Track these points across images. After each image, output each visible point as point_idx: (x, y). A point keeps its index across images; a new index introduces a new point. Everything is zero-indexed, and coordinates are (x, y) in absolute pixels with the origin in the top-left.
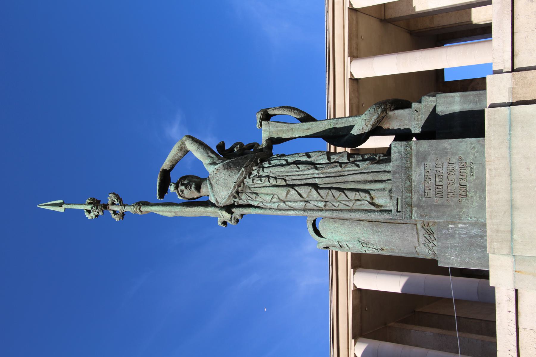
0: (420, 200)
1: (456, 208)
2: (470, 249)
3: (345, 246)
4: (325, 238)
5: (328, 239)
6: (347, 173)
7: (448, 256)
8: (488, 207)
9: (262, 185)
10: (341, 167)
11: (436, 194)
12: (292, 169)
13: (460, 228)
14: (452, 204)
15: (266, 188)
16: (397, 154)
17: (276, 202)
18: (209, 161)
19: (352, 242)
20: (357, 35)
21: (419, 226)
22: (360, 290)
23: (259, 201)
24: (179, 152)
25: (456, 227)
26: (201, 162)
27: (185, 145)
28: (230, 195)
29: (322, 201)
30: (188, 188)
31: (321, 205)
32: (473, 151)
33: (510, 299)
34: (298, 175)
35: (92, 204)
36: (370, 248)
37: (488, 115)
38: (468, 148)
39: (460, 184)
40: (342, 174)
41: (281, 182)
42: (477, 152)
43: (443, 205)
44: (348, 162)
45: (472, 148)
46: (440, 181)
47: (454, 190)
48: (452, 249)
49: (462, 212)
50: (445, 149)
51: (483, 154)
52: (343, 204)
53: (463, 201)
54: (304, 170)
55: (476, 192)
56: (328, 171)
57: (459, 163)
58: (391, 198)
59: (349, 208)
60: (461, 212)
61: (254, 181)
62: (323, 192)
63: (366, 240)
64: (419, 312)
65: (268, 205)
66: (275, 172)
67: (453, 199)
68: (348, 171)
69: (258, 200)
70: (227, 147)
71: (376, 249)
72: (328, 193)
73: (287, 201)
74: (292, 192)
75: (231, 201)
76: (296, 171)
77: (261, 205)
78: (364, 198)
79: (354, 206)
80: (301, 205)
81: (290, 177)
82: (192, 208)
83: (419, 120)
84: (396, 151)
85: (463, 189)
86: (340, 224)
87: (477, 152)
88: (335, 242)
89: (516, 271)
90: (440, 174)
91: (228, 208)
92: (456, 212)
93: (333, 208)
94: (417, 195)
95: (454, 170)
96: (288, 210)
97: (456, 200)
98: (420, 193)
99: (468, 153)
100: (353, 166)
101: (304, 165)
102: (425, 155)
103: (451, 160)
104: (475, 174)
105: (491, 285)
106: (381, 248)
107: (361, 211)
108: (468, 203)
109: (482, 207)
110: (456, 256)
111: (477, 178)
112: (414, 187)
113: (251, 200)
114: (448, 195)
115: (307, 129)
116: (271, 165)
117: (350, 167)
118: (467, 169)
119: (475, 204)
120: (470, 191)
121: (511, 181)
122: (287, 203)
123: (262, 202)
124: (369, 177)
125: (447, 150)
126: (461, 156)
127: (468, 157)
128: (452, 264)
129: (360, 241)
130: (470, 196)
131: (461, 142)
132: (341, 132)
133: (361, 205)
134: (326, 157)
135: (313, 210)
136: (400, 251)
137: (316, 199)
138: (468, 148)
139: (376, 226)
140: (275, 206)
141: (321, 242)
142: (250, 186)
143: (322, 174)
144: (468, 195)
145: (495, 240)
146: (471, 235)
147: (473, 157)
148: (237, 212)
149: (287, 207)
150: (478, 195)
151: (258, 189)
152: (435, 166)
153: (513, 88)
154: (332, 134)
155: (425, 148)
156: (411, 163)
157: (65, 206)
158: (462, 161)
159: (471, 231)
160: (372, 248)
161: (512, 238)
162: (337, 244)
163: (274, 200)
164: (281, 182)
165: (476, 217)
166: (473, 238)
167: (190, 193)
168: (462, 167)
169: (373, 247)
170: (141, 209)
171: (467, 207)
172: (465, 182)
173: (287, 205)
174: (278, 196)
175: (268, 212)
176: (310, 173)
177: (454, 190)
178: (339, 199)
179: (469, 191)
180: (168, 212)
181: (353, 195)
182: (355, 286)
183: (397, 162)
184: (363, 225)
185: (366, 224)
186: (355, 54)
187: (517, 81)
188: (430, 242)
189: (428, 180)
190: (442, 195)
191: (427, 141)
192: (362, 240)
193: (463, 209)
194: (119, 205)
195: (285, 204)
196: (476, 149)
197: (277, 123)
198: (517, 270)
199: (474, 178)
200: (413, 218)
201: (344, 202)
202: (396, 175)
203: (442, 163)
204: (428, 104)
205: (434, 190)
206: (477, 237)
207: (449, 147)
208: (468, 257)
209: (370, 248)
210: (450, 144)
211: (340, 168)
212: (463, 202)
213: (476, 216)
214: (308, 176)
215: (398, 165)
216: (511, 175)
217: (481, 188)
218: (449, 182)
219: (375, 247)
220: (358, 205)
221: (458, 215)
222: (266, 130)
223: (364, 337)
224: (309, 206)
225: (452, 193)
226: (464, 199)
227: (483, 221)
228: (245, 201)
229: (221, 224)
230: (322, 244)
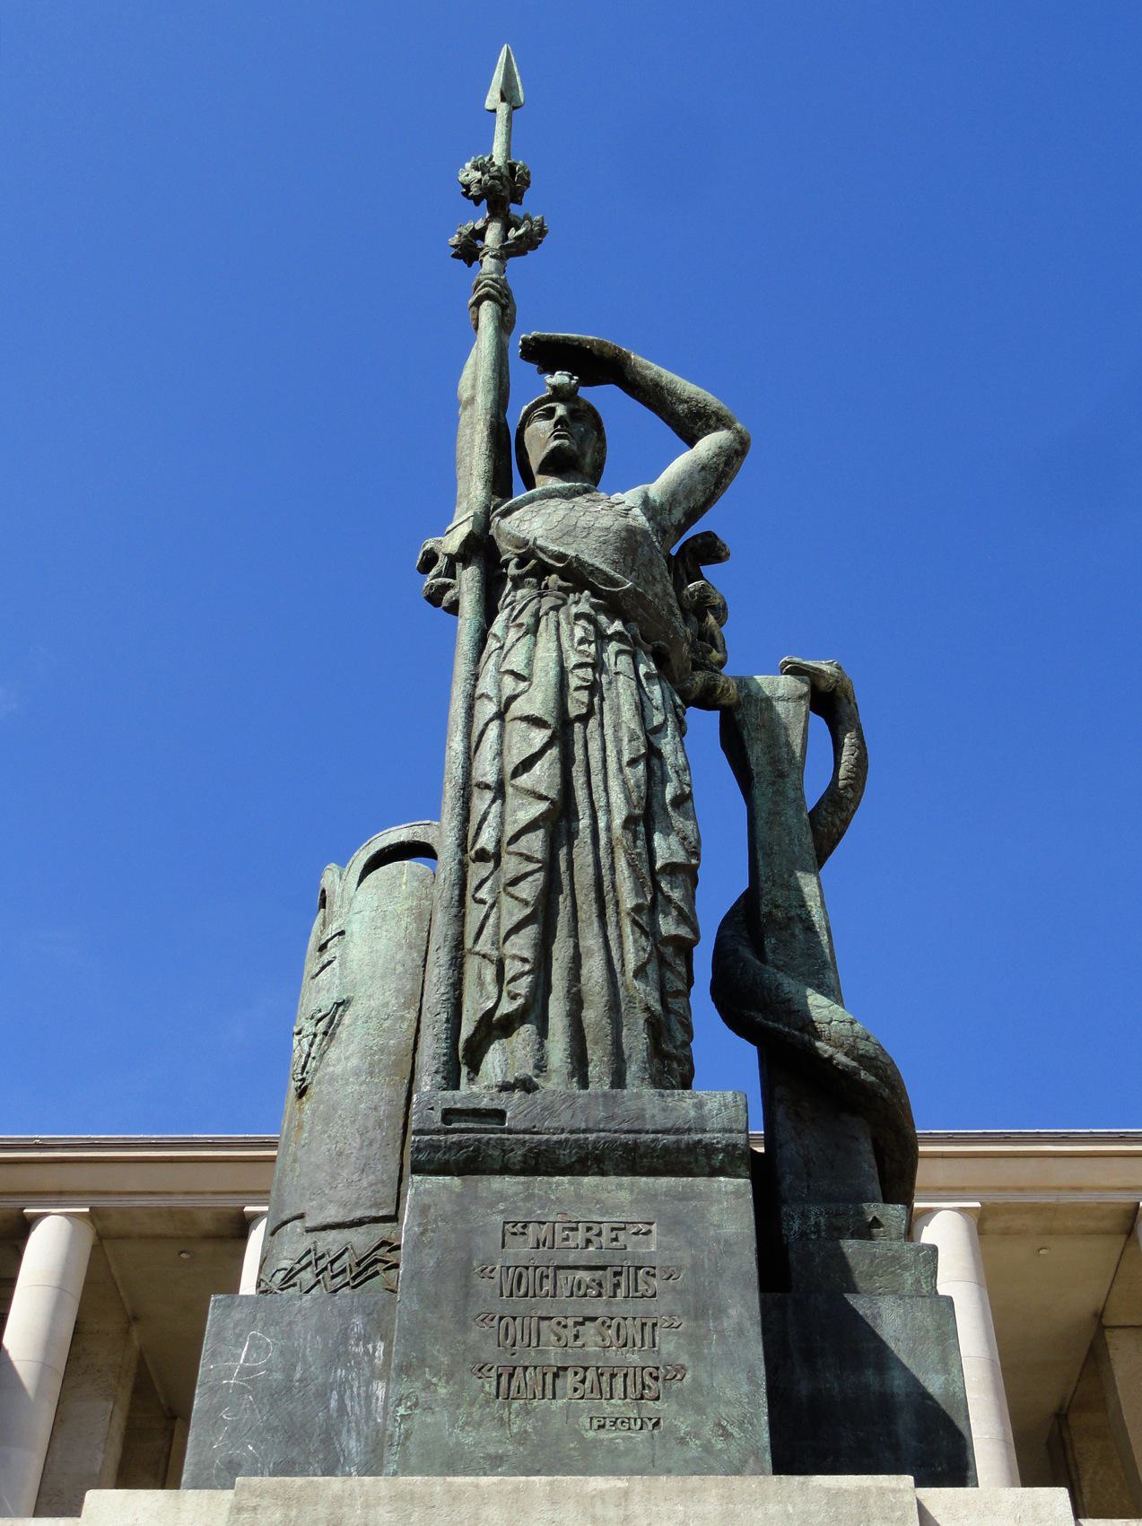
0: (491, 1205)
1: (452, 1355)
2: (275, 1429)
3: (326, 957)
4: (358, 885)
5: (355, 896)
6: (612, 933)
7: (254, 1337)
8: (451, 1484)
9: (566, 644)
10: (637, 909)
11: (517, 1267)
12: (630, 741)
13: (368, 1389)
14: (474, 1335)
15: (555, 654)
16: (692, 1113)
17: (500, 690)
18: (656, 498)
20: (1050, 1232)
23: (505, 639)
24: (689, 408)
25: (373, 1372)
26: (652, 480)
28: (531, 543)
29: (499, 842)
31: (486, 840)
32: (707, 1430)
34: (604, 761)
35: (508, 175)
36: (311, 1045)
37: (882, 1492)
38: (723, 1410)
40: (610, 910)
41: (577, 702)
42: (707, 1448)
43: (467, 1295)
44: (658, 865)
45: (724, 1428)
46: (575, 1289)
47: (534, 1343)
48: (282, 1353)
49: (434, 1380)
50: (721, 1311)
51: (701, 1467)
52: (487, 917)
53: (483, 1386)
54: (624, 783)
55: (522, 1438)
56: (622, 864)
57: (657, 1368)
58: (506, 1087)
59: (469, 943)
60: (435, 1376)
61: (582, 622)
62: (535, 843)
63: (342, 1033)
64: (173, 1431)
65: (489, 668)
66: (617, 689)
67: (492, 1342)
68: (620, 936)
69: (510, 634)
71: (304, 1067)
72: (529, 859)
73: (502, 728)
74: (539, 737)
75: (508, 552)
76: (619, 753)
77: (492, 644)
78: (509, 993)
79: (477, 959)
80: (486, 770)
82: (486, 439)
85: (536, 1383)
86: (410, 933)
87: (707, 1448)
88: (340, 921)
90: (608, 1287)
91: (480, 548)
92: (436, 1353)
93: (472, 883)
94: (516, 1194)
95: (625, 1345)
96: (468, 735)
97: (489, 1352)
99: (700, 1410)
100: (641, 953)
101: (642, 781)
102: (690, 1227)
103: (668, 1334)
104: (603, 1435)
105: (93, 1498)
106: (306, 1087)
107: (457, 986)
110: (248, 1367)
111: (587, 1448)
113: (510, 615)
114: (514, 1319)
116: (642, 678)
117: (635, 941)
118: (628, 1400)
120: (528, 1413)
122: (493, 731)
123: (501, 648)
124: (593, 1014)
125: (715, 1319)
126: (688, 1376)
127: (682, 1406)
128: (213, 1354)
129: (341, 1008)
130: (506, 1415)
131: (751, 1380)
132: (773, 941)
133: (481, 983)
134: (675, 860)
135: (466, 820)
136: (289, 1159)
137: (509, 819)
138: (723, 1410)
139: (397, 1064)
140: (486, 685)
141: (345, 873)
142: (563, 609)
143: (610, 841)
144: (510, 1406)
145: (294, 1513)
146: (338, 1433)
147: (683, 1429)
148: (468, 581)
149: (481, 727)
150: (510, 1447)
151: (553, 632)
152: (640, 1268)
154: (764, 909)
155: (719, 1226)
157: (503, 109)
158: (665, 1380)
159: (354, 1435)
160: (309, 1055)
164: (577, 702)
165: (407, 1438)
166: (322, 1441)
167: (541, 438)
168: (639, 1381)
169: (312, 1055)
170: (486, 303)
171: (454, 1402)
172: (570, 1392)
173: (487, 724)
174: (523, 692)
175: (462, 668)
176: (613, 798)
177: (534, 1343)
178: (505, 900)
179: (527, 1412)
180: (475, 379)
181: (520, 949)
183: (656, 1111)
184: (402, 1017)
185: (407, 1027)
186: (989, 1225)
188: (318, 1275)
189: (580, 1236)
190: (511, 1295)
191: (753, 1234)
192: (341, 1016)
193: (447, 1382)
194: (503, 242)
195: (491, 720)
197: (802, 724)
199: (587, 1431)
201: (491, 920)
202: (601, 1108)
203: (654, 1296)
204: (905, 1268)
206: (325, 1459)
207: (727, 1324)
208: (241, 1419)
209: (311, 1045)
210: (740, 1331)
211: (632, 905)
213: (412, 1439)
214: (599, 795)
215: (643, 1116)
218: (570, 1322)
219: (312, 1064)
220: (479, 973)
221: (422, 1362)
223: (94, 1247)
224: (481, 801)
225: (519, 1337)
226: (490, 1387)
228: (508, 600)
229: (428, 547)
230: (337, 880)
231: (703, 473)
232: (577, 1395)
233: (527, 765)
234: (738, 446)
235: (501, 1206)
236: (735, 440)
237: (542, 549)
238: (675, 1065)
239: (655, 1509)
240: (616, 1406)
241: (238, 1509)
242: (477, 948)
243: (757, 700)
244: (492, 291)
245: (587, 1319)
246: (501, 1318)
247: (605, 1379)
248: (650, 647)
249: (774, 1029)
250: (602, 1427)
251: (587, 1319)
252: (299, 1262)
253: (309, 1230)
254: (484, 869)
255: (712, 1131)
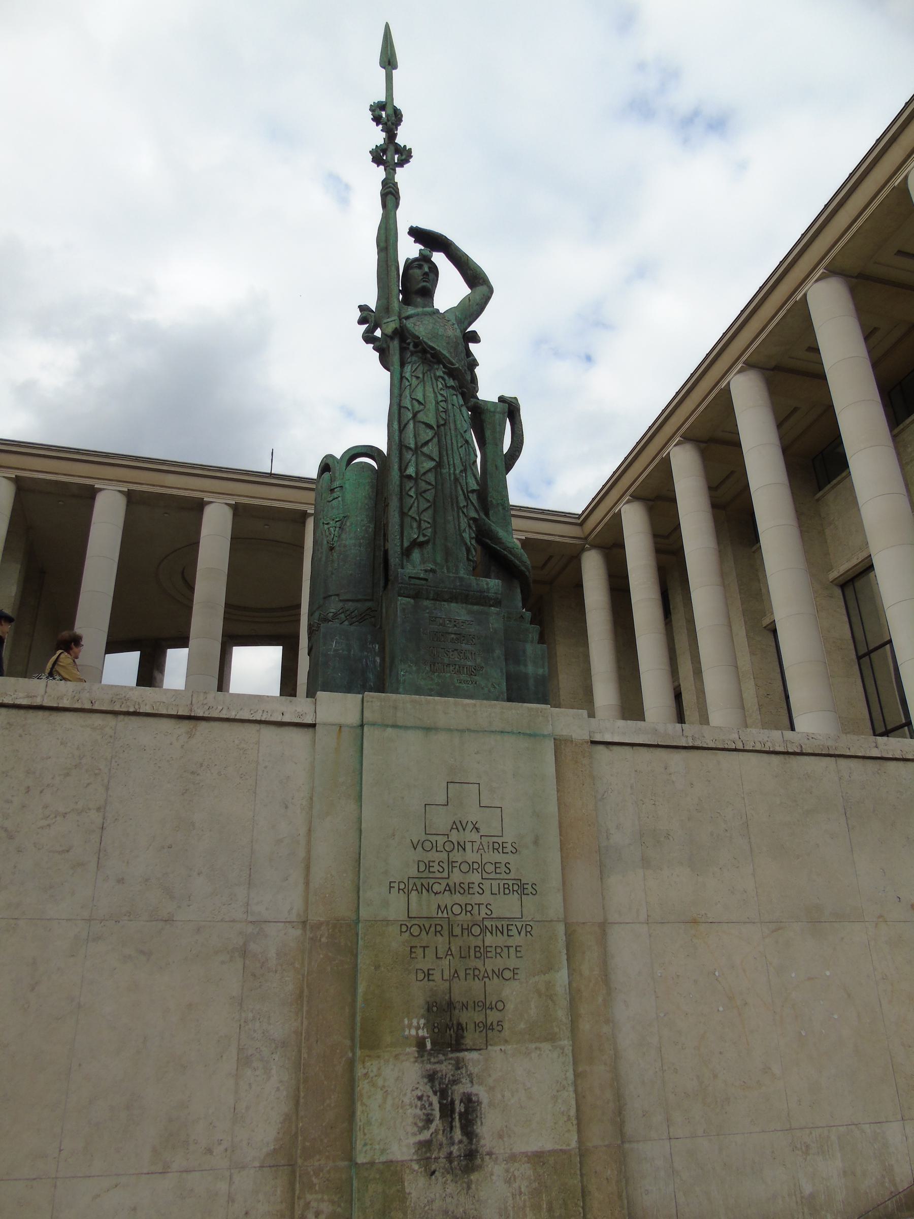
3: (335, 495)
7: (336, 639)
9: (436, 390)
19: (341, 507)
21: (369, 604)
27: (482, 285)
30: (425, 277)
33: (301, 717)
42: (489, 691)
49: (412, 665)
52: (414, 503)
53: (426, 668)
72: (429, 484)
79: (409, 519)
81: (449, 433)
84: (490, 585)
87: (489, 691)
89: (340, 727)
98: (433, 611)
104: (460, 685)
106: (333, 548)
108: (423, 673)
109: (418, 691)
112: (441, 604)
115: (496, 466)
119: (423, 683)
121: (462, 731)
126: (484, 670)
156: (473, 604)
161: (387, 726)
162: (337, 484)
163: (416, 403)
165: (405, 681)
182: (100, 490)
184: (369, 526)
187: (580, 747)
195: (410, 419)
196: (492, 690)
198: (343, 729)
200: (400, 598)
201: (416, 504)
212: (425, 666)
217: (444, 691)
218: (451, 650)
227: (401, 690)
231: (477, 306)
232: (453, 673)
233: (426, 443)
235: (428, 611)
237: (426, 343)
238: (472, 563)
240: (463, 677)
242: (410, 514)
244: (393, 191)
247: (461, 668)
249: (494, 548)
250: (461, 682)
252: (339, 611)
253: (341, 601)
254: (411, 484)
255: (491, 593)
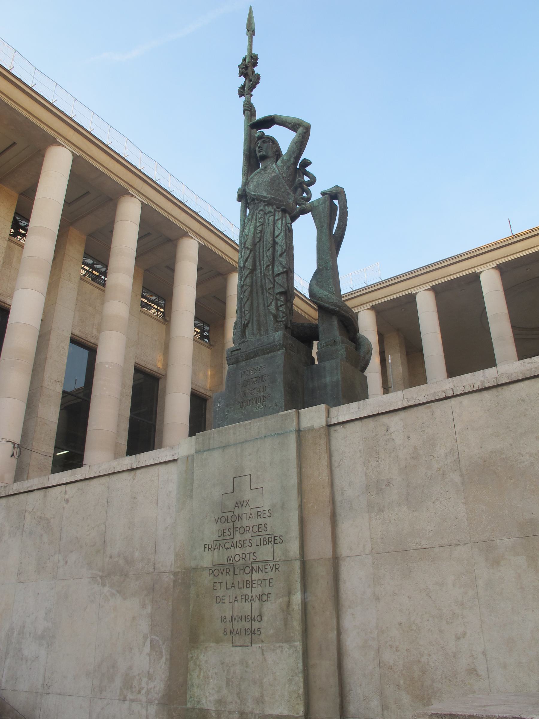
22: (415, 300)
27: (299, 128)
39: (251, 400)
42: (273, 409)
45: (276, 404)
70: (307, 169)
83: (327, 346)
95: (261, 392)
104: (257, 410)
121: (241, 443)
153: (313, 429)
205: (246, 379)
216: (246, 441)
218: (252, 390)
222: (320, 202)
234: (305, 131)
236: (304, 129)
239: (254, 425)
240: (259, 404)
241: (196, 439)
243: (316, 207)
245: (255, 388)
246: (241, 392)
248: (280, 210)
251: (255, 388)
